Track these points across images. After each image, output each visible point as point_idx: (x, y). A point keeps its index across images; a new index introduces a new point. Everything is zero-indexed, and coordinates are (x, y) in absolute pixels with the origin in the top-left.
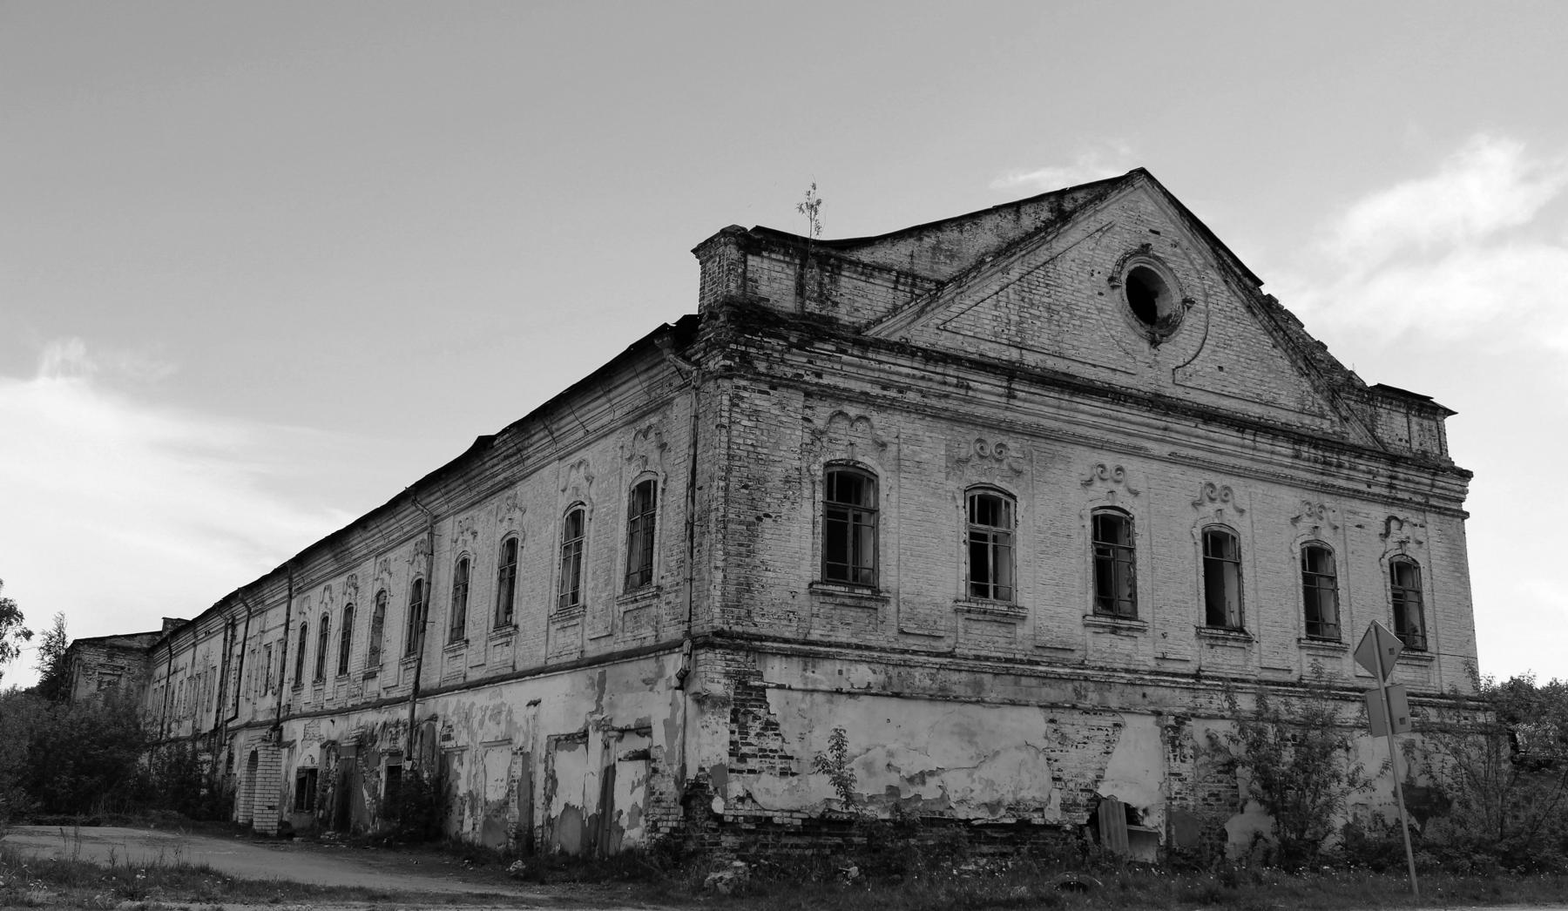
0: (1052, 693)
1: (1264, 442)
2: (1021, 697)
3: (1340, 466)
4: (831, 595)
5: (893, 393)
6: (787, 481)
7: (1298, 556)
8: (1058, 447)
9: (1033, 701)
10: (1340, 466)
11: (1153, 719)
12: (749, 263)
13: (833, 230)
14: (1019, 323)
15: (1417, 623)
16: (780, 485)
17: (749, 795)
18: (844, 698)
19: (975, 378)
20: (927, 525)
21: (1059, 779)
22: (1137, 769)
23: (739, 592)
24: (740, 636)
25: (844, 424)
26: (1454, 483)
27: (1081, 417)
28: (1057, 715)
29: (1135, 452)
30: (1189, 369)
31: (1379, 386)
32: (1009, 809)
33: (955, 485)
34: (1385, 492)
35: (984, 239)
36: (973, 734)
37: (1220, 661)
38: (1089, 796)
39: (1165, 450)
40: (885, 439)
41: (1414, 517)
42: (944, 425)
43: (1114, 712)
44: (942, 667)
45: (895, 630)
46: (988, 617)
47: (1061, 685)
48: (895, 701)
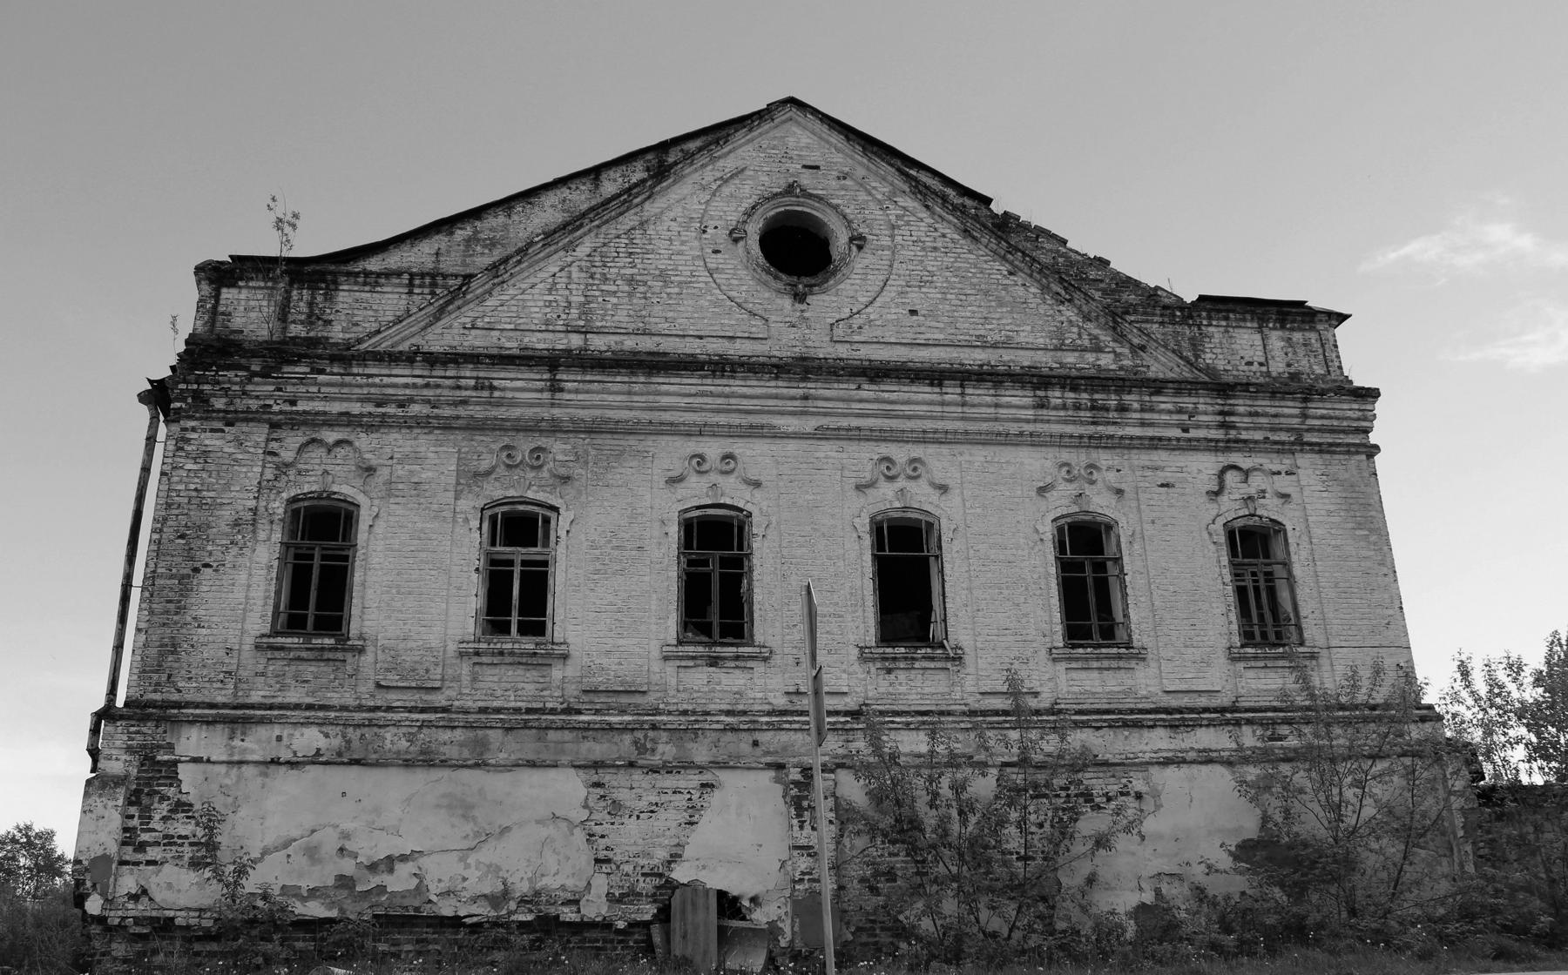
0: (597, 749)
1: (980, 395)
2: (547, 757)
3: (1122, 409)
4: (282, 648)
5: (391, 409)
6: (237, 524)
7: (1048, 537)
8: (632, 441)
9: (565, 759)
10: (1122, 409)
11: (772, 773)
13: (308, 244)
15: (1289, 609)
16: (227, 529)
17: (145, 892)
18: (283, 769)
19: (502, 375)
20: (423, 555)
21: (608, 861)
22: (740, 842)
23: (161, 654)
25: (321, 452)
26: (1349, 409)
27: (665, 400)
28: (606, 777)
29: (753, 432)
31: (1202, 298)
32: (523, 901)
33: (470, 504)
34: (1217, 434)
35: (548, 213)
36: (472, 807)
37: (903, 689)
38: (657, 882)
39: (809, 424)
40: (374, 462)
42: (459, 435)
43: (701, 769)
45: (371, 685)
46: (508, 659)
47: (619, 736)
48: (355, 768)
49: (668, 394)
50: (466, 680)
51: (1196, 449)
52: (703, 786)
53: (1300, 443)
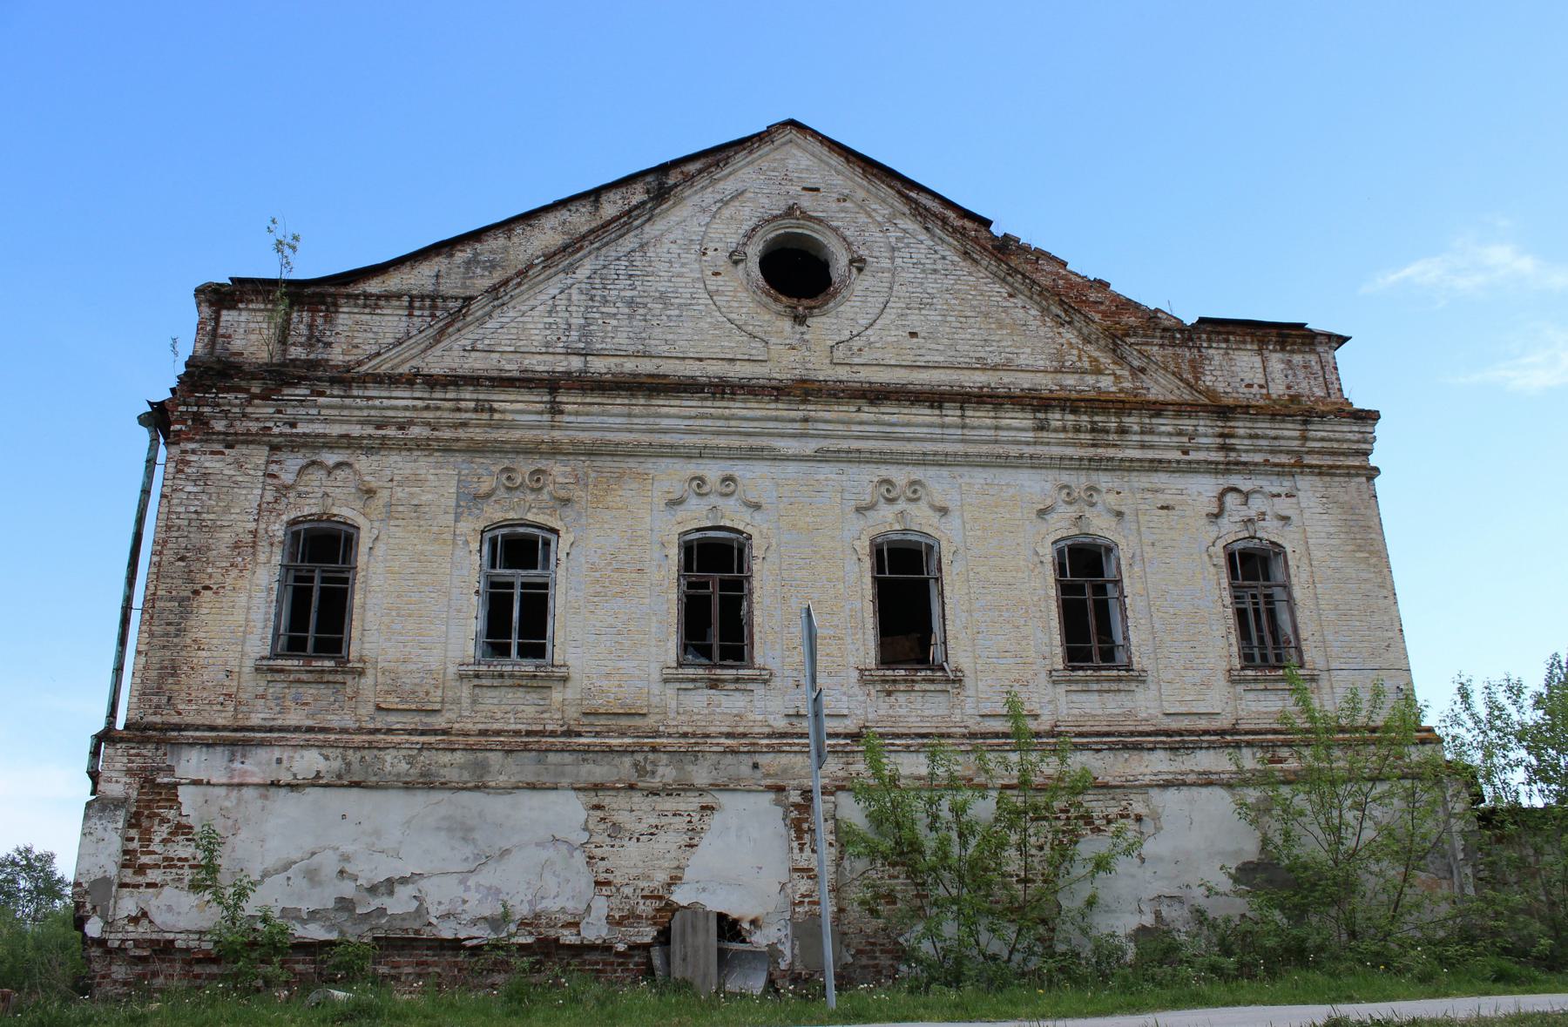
0: (598, 771)
1: (980, 417)
2: (547, 779)
3: (1123, 431)
4: (282, 671)
5: (391, 432)
6: (236, 546)
7: (1048, 559)
10: (1123, 431)
11: (772, 796)
12: (223, 318)
13: (307, 268)
14: (583, 327)
17: (145, 914)
18: (283, 791)
19: (502, 397)
20: (423, 577)
21: (608, 883)
22: (740, 864)
23: (161, 677)
24: (152, 726)
25: (321, 474)
26: (1348, 431)
27: (665, 422)
28: (606, 799)
29: (754, 454)
30: (857, 343)
32: (523, 924)
33: (470, 527)
34: (1218, 456)
35: (547, 236)
36: (471, 829)
37: (903, 712)
38: (657, 904)
40: (374, 485)
41: (1271, 484)
42: (459, 458)
43: (701, 791)
44: (424, 747)
45: (371, 708)
46: (508, 682)
47: (618, 758)
48: (355, 791)
49: (667, 416)
50: (466, 702)
52: (703, 808)
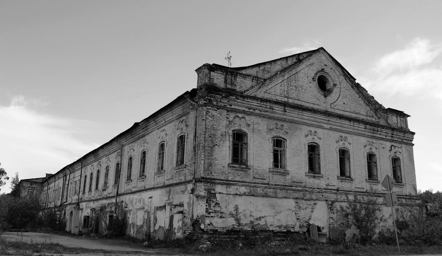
0: (297, 195)
1: (356, 124)
2: (288, 196)
3: (378, 131)
4: (234, 167)
5: (252, 111)
6: (222, 135)
7: (366, 156)
8: (298, 126)
9: (291, 197)
10: (378, 131)
11: (325, 202)
12: (211, 74)
13: (235, 64)
14: (287, 91)
15: (399, 175)
16: (220, 136)
17: (211, 223)
18: (238, 196)
19: (275, 106)
20: (261, 147)
21: (299, 219)
22: (320, 216)
23: (208, 166)
24: (209, 179)
25: (238, 119)
26: (410, 136)
27: (305, 117)
29: (320, 127)
30: (335, 104)
31: (389, 108)
33: (269, 136)
34: (390, 138)
35: (277, 67)
38: (307, 224)
39: (328, 126)
40: (250, 123)
42: (266, 119)
43: (314, 200)
44: (265, 187)
45: (252, 177)
46: (279, 173)
47: (299, 192)
48: (252, 197)
49: (305, 116)
50: (271, 177)
51: (387, 141)
52: (314, 204)
53: (402, 142)
